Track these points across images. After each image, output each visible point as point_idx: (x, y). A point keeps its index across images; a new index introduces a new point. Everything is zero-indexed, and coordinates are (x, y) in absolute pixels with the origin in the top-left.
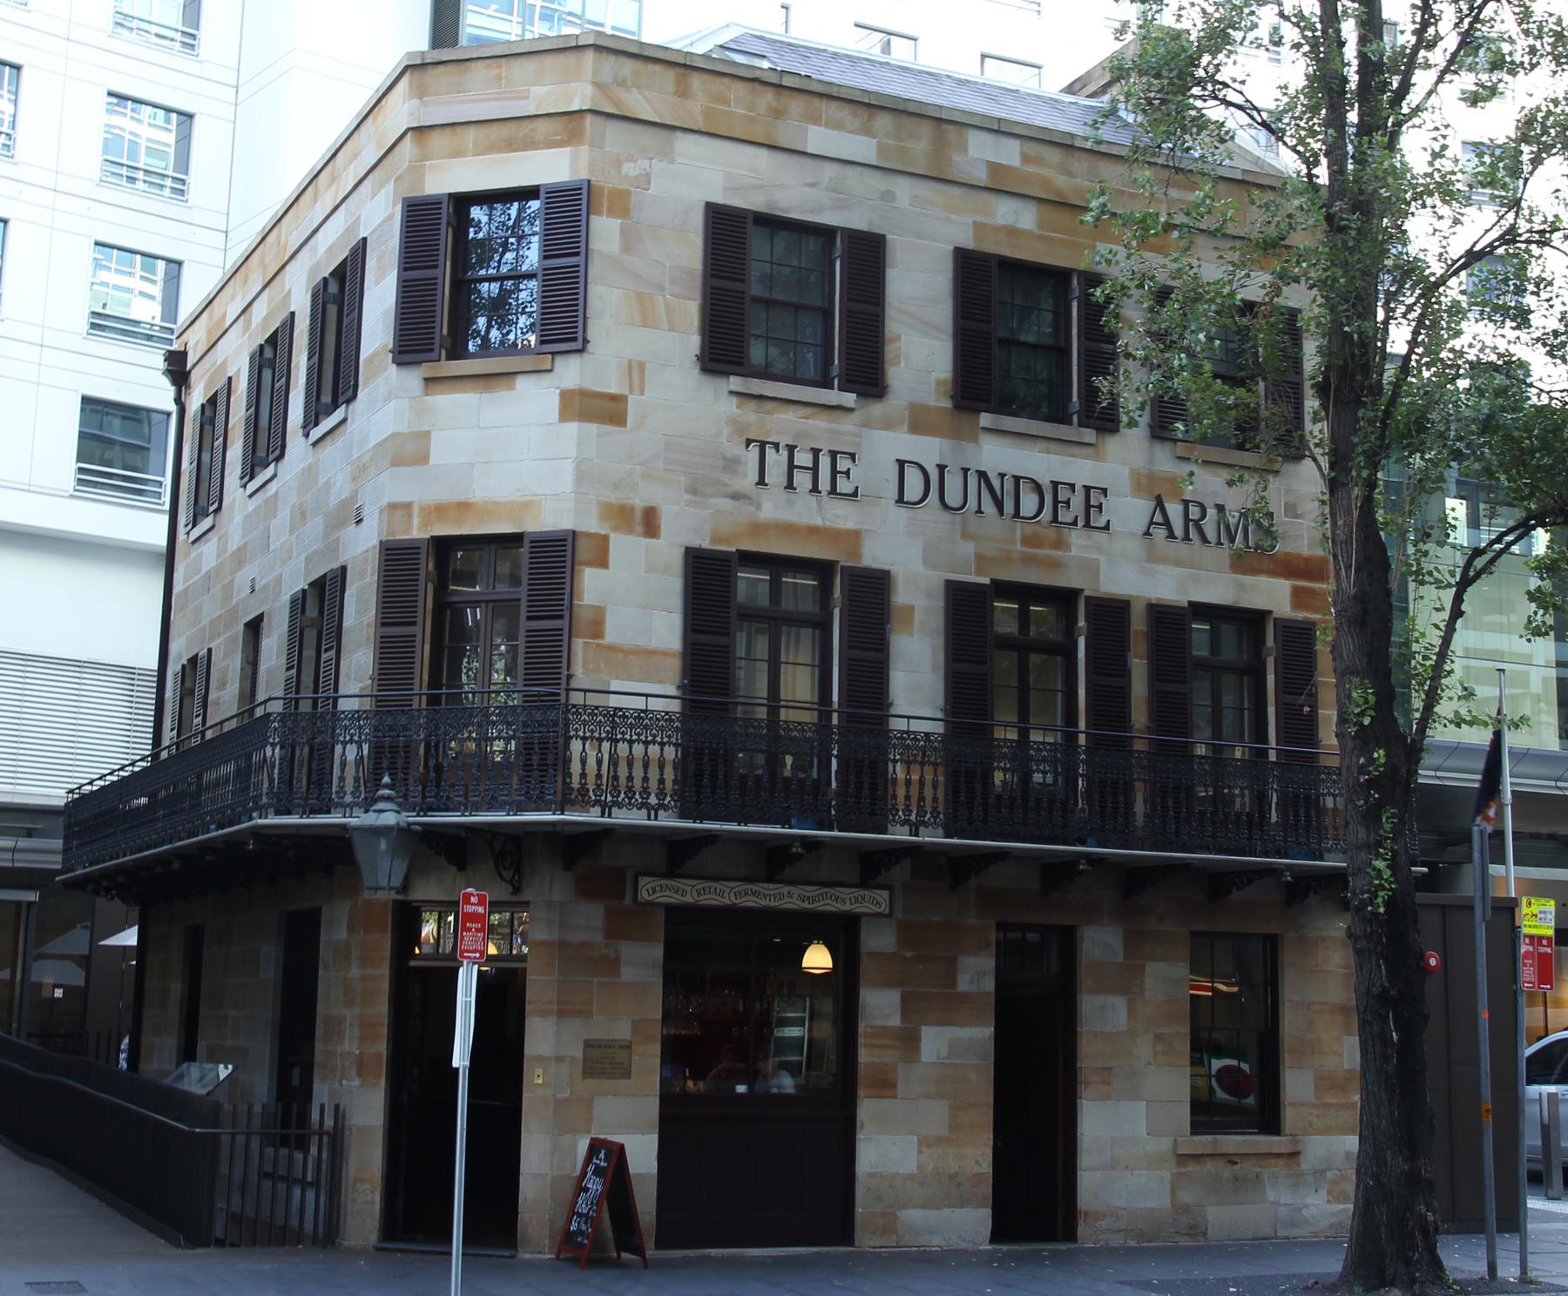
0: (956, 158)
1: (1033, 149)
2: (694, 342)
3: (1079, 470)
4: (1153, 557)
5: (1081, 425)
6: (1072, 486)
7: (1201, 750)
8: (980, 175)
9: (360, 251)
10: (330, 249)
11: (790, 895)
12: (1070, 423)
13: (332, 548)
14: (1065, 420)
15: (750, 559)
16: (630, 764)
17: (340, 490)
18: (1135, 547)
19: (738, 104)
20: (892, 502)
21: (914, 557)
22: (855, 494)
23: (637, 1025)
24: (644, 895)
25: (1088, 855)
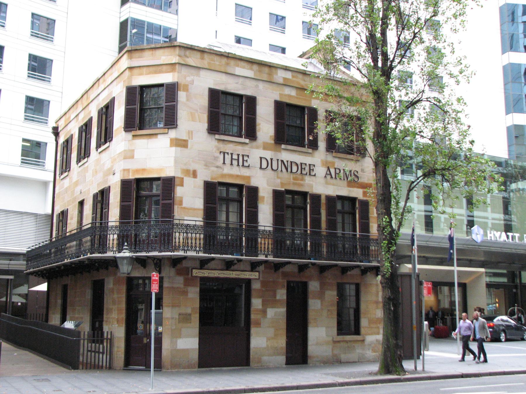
0: (275, 76)
1: (295, 74)
2: (206, 125)
3: (307, 160)
4: (327, 183)
5: (308, 148)
6: (306, 164)
7: (288, 230)
8: (281, 81)
9: (113, 101)
10: (103, 100)
11: (233, 274)
12: (305, 147)
13: (106, 181)
14: (304, 146)
15: (221, 184)
16: (192, 239)
17: (108, 165)
18: (323, 181)
19: (218, 62)
20: (258, 169)
21: (266, 184)
22: (249, 166)
23: (193, 309)
24: (194, 274)
25: (311, 263)
